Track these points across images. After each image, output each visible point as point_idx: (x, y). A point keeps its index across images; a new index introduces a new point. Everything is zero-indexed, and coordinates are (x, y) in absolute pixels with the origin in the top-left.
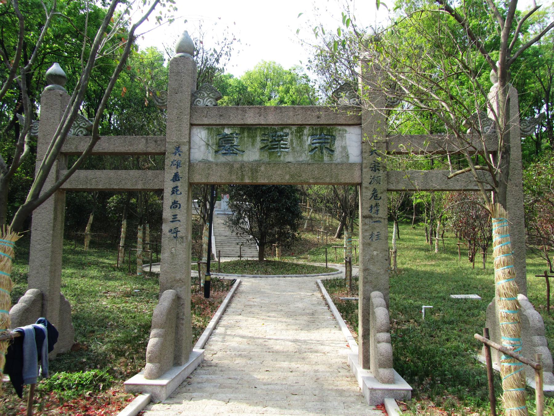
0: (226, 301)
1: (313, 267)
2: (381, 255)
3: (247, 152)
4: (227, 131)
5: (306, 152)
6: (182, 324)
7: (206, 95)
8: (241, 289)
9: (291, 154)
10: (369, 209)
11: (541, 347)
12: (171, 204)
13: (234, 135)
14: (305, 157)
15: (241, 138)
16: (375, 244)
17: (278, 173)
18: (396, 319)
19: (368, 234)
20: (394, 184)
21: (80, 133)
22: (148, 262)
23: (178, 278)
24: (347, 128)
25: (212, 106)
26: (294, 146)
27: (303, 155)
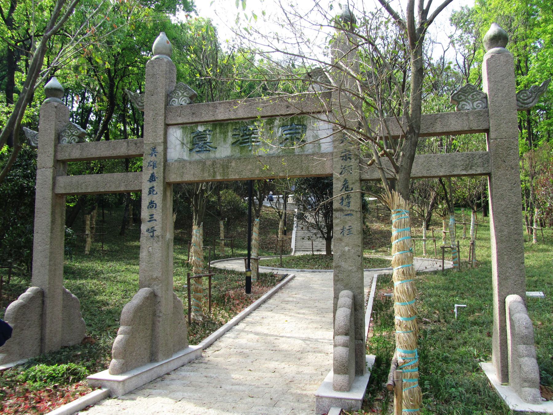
0: (264, 297)
3: (219, 148)
4: (201, 129)
6: (159, 322)
7: (180, 94)
10: (340, 201)
11: (526, 358)
12: (148, 204)
13: (207, 132)
14: (275, 149)
15: (214, 134)
17: (249, 168)
20: (369, 173)
21: (73, 141)
23: (154, 276)
25: (186, 104)
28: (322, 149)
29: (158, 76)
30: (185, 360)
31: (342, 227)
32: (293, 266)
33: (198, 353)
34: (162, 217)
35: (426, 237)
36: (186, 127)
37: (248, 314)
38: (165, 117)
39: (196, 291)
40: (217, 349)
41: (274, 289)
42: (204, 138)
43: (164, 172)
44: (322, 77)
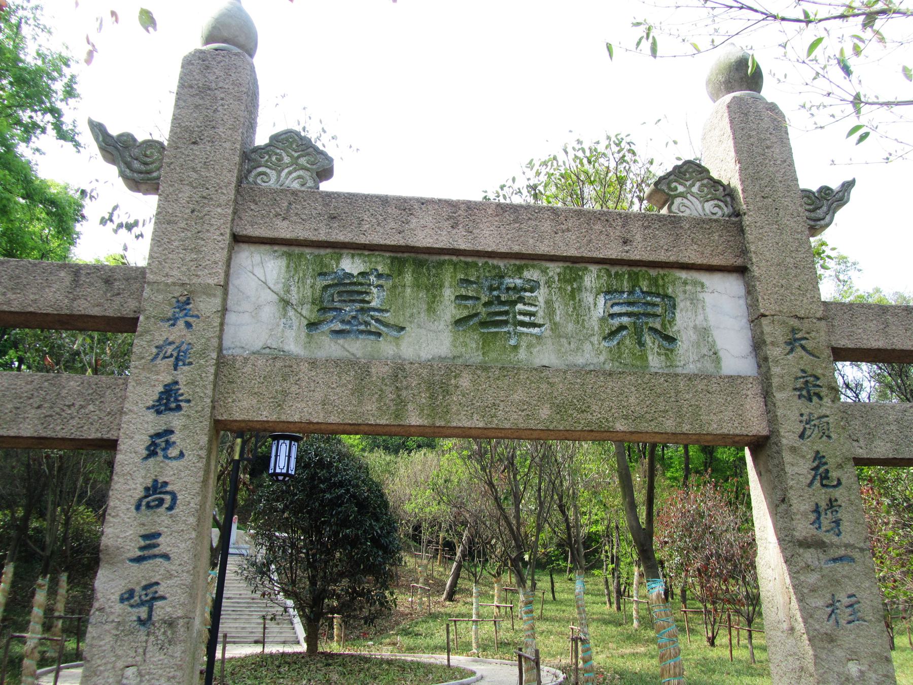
4: (351, 265)
5: (595, 339)
7: (287, 160)
9: (549, 342)
10: (812, 517)
12: (139, 493)
14: (592, 353)
15: (394, 287)
19: (820, 603)
20: (862, 443)
22: (51, 662)
24: (704, 278)
26: (557, 319)
27: (587, 347)
28: (724, 364)
29: (219, 94)
31: (829, 596)
35: (478, 614)
36: (301, 255)
42: (361, 293)
44: (703, 185)
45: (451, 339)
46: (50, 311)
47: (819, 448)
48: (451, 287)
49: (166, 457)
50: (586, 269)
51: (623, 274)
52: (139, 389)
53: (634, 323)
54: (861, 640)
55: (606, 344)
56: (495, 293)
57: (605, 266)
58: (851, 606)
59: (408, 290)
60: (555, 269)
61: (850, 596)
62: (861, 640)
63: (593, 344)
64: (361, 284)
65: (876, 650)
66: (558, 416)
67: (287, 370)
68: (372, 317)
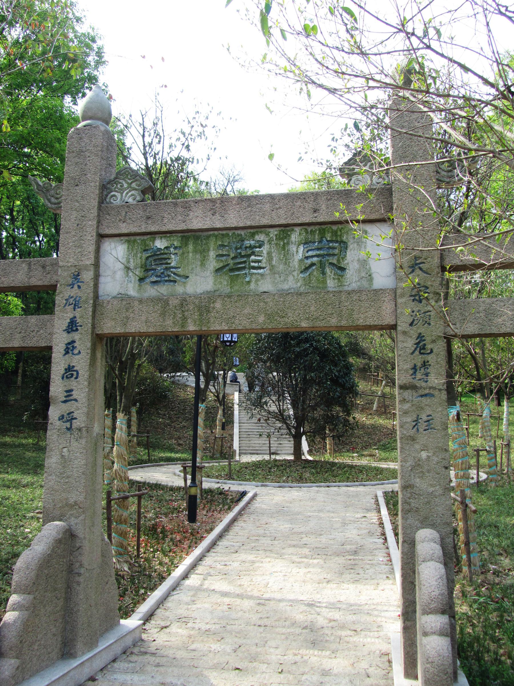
1: (377, 469)
2: (436, 459)
3: (192, 277)
4: (160, 244)
5: (295, 274)
6: (78, 583)
7: (125, 185)
8: (256, 504)
10: (411, 372)
12: (63, 371)
13: (172, 249)
14: (293, 282)
15: (183, 253)
16: (423, 438)
17: (246, 311)
18: (496, 564)
19: (409, 420)
23: (72, 501)
24: (368, 227)
26: (274, 263)
27: (291, 278)
30: (118, 649)
31: (415, 416)
32: (248, 477)
33: (137, 634)
34: (89, 395)
36: (135, 241)
37: (201, 558)
38: (99, 222)
39: (120, 521)
40: (163, 624)
41: (231, 515)
42: (166, 259)
43: (94, 317)
45: (213, 281)
46: (20, 285)
47: (421, 331)
48: (214, 250)
49: (73, 354)
50: (293, 230)
51: (315, 231)
52: (60, 321)
53: (321, 261)
54: (430, 440)
55: (302, 276)
56: (239, 251)
57: (304, 227)
58: (428, 421)
59: (191, 255)
60: (273, 232)
61: (428, 416)
62: (430, 440)
63: (294, 276)
64: (166, 254)
65: (439, 445)
66: (269, 321)
67: (128, 305)
68: (172, 272)
